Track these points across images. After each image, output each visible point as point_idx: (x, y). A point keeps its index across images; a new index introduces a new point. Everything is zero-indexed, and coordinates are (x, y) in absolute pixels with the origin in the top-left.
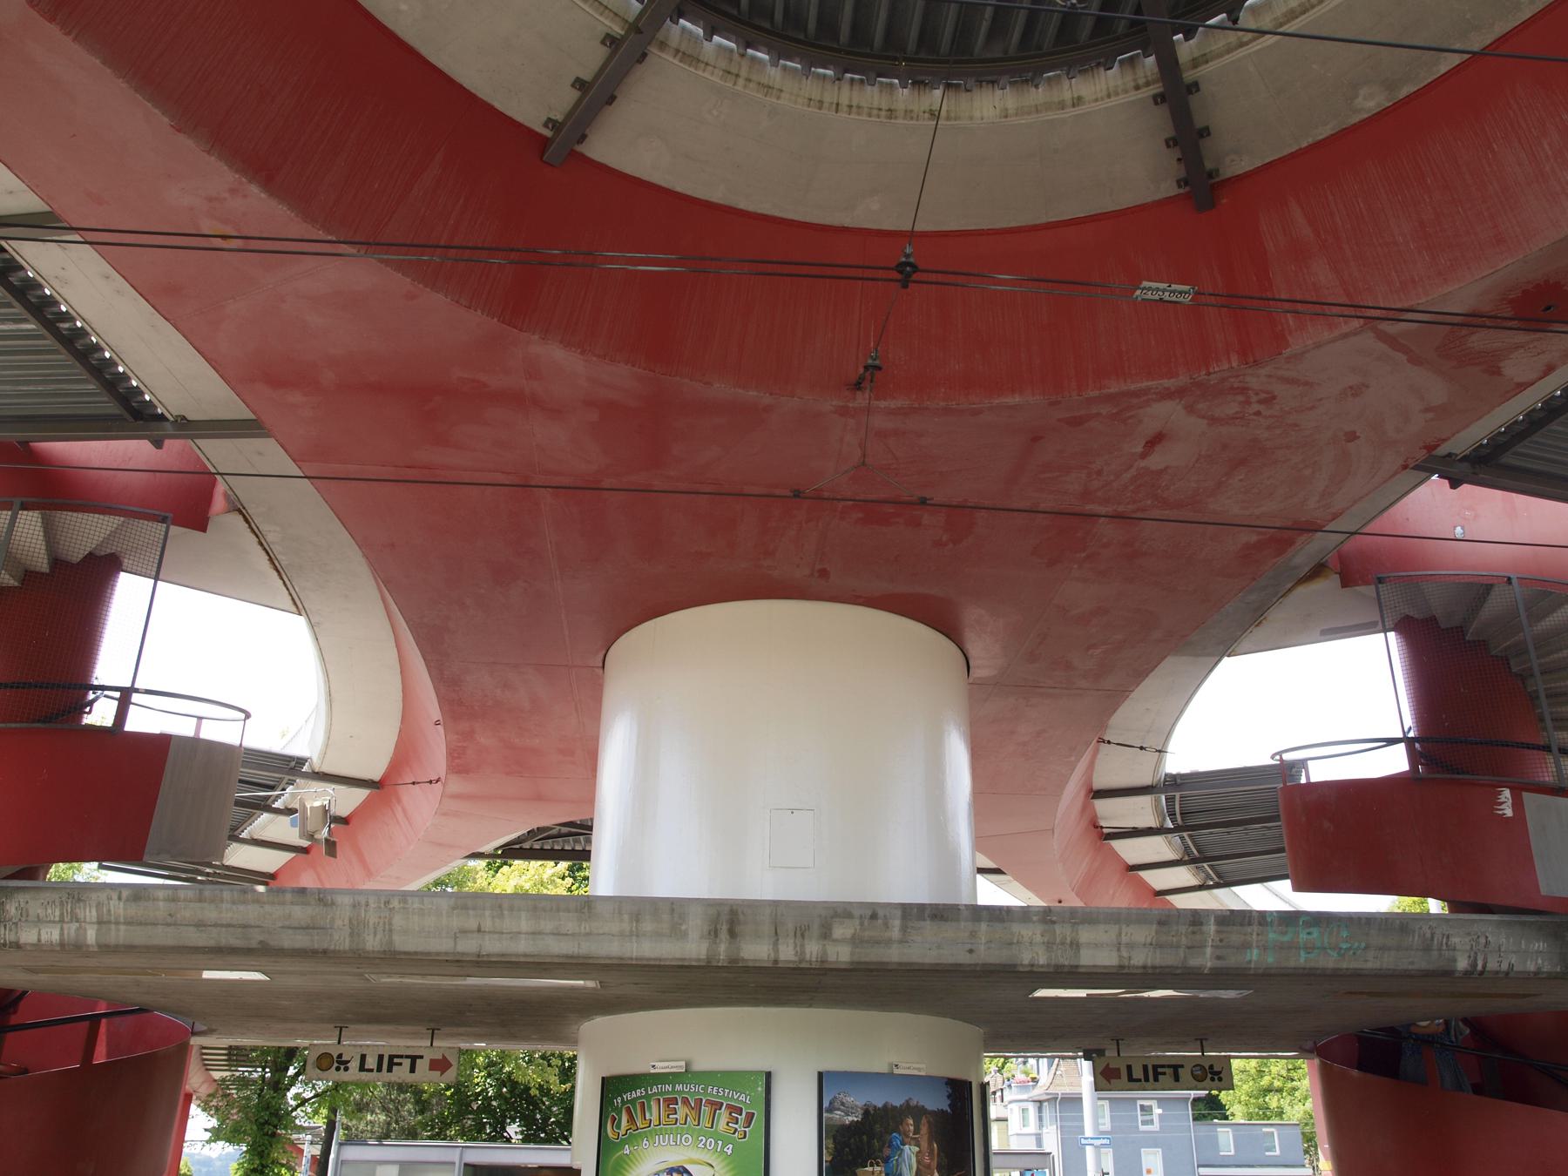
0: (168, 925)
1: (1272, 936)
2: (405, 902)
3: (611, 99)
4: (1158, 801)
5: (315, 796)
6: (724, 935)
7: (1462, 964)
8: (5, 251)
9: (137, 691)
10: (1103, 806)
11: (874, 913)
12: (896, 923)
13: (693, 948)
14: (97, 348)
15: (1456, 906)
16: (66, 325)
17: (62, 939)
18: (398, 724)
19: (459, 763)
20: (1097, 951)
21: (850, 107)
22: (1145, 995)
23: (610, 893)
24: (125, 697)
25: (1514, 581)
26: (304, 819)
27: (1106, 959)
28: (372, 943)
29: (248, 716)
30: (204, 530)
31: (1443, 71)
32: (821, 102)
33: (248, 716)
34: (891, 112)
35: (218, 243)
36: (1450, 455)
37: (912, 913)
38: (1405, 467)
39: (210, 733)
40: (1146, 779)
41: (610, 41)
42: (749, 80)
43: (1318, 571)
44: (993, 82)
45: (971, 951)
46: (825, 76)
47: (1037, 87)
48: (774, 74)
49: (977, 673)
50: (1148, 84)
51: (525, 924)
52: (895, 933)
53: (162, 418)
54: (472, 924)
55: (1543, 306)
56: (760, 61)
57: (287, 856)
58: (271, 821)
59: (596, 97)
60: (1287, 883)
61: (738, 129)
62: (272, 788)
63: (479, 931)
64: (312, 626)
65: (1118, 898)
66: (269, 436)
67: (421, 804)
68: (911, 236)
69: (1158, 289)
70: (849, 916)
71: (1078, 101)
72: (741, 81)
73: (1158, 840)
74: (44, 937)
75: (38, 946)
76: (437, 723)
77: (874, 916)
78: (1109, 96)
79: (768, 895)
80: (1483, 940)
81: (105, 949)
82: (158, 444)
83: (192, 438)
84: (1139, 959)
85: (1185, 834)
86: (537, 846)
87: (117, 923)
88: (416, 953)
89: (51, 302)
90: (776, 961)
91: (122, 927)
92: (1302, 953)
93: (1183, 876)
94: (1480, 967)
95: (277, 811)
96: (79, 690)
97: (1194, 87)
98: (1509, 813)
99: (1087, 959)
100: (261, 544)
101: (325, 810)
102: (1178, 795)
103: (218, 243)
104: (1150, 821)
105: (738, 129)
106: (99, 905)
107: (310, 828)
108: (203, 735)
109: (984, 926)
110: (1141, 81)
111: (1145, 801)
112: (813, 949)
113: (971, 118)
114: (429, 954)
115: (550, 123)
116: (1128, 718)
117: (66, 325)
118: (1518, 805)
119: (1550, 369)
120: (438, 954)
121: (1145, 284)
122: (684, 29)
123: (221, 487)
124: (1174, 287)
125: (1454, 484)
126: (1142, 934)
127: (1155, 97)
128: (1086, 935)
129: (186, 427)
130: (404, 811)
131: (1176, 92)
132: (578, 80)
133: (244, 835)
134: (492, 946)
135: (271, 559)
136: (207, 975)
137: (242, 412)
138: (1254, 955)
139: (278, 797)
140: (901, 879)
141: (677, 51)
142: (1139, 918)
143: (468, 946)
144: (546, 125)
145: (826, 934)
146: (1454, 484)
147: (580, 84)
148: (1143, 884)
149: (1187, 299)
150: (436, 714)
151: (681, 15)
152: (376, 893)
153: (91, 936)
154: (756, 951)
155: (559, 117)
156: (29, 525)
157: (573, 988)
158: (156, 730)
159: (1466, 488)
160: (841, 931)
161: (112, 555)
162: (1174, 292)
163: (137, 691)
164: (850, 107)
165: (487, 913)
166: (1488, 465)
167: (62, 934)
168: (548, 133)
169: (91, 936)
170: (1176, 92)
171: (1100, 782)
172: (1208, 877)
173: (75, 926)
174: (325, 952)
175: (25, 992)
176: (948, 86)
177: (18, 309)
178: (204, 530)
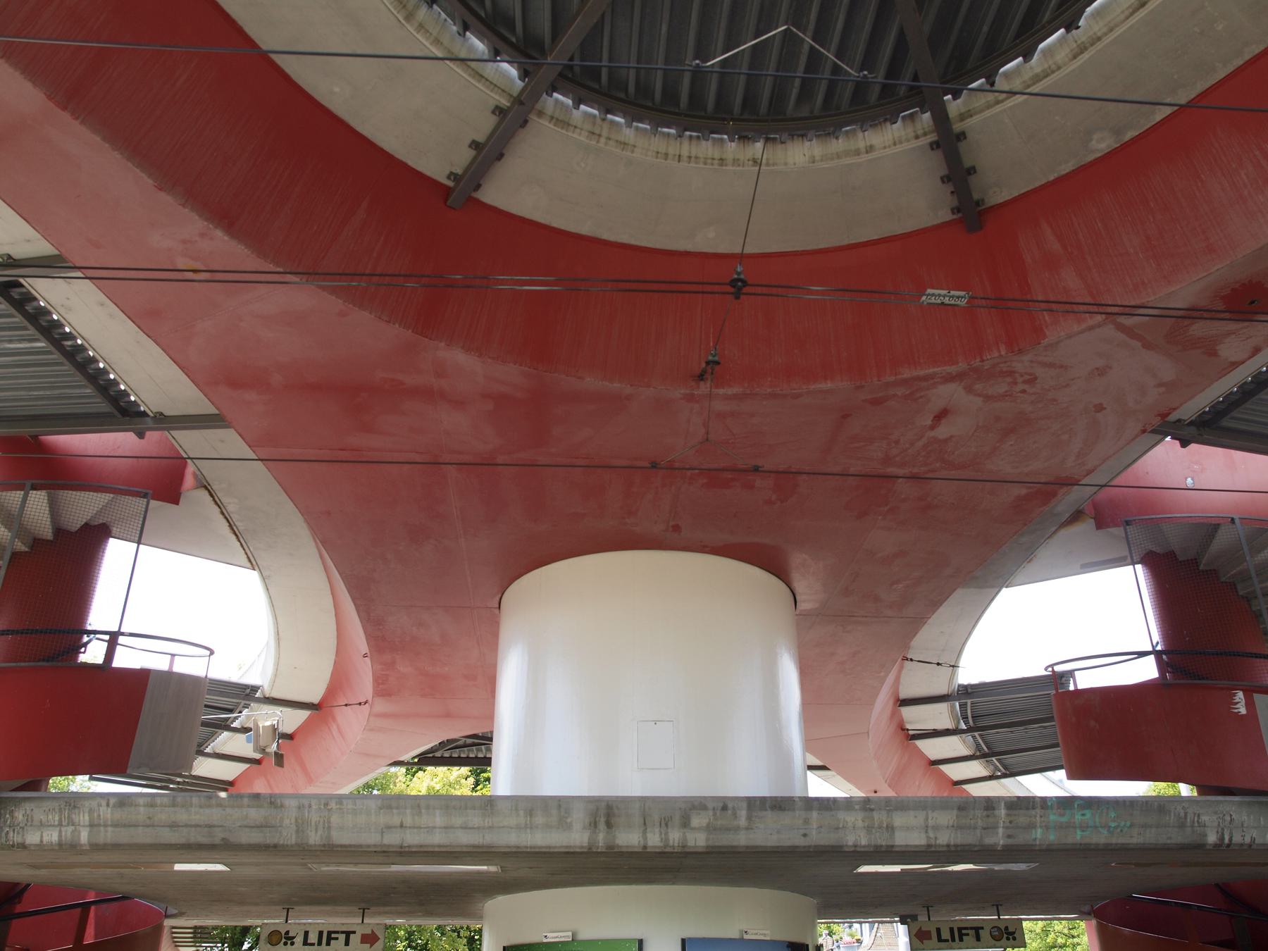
0: (148, 826)
1: (1052, 817)
2: (341, 803)
3: (500, 156)
4: (953, 707)
5: (266, 717)
6: (602, 826)
7: (1212, 838)
8: (22, 286)
9: (123, 634)
10: (907, 712)
11: (724, 805)
12: (743, 813)
13: (577, 837)
14: (94, 360)
15: (1204, 789)
19: (383, 688)
20: (909, 833)
21: (690, 157)
22: (949, 869)
24: (113, 639)
25: (1237, 521)
26: (257, 735)
27: (916, 839)
28: (314, 838)
29: (212, 652)
30: (175, 500)
32: (666, 155)
33: (212, 652)
34: (722, 161)
35: (190, 275)
38: (1144, 431)
39: (181, 667)
40: (943, 690)
41: (499, 111)
42: (609, 139)
43: (1076, 516)
44: (802, 136)
45: (805, 835)
46: (669, 134)
47: (837, 138)
48: (628, 134)
49: (803, 606)
50: (925, 134)
51: (439, 820)
52: (743, 822)
53: (144, 414)
54: (396, 820)
55: (1249, 300)
56: (617, 124)
58: (230, 738)
59: (489, 153)
61: (597, 175)
62: (231, 711)
63: (401, 826)
64: (264, 579)
65: (924, 789)
67: (351, 722)
71: (870, 149)
72: (603, 140)
74: (46, 839)
75: (41, 847)
77: (725, 808)
78: (895, 144)
80: (1228, 818)
81: (96, 847)
82: (141, 435)
83: (168, 429)
84: (944, 839)
86: (447, 755)
87: (105, 826)
88: (350, 846)
90: (645, 847)
91: (110, 829)
93: (976, 768)
94: (1227, 841)
95: (235, 730)
97: (962, 136)
98: (1243, 711)
100: (222, 513)
101: (274, 729)
102: (969, 702)
103: (190, 275)
104: (947, 724)
105: (597, 175)
106: (91, 811)
107: (262, 743)
108: (176, 669)
109: (815, 814)
110: (920, 132)
111: (943, 707)
112: (675, 836)
113: (786, 164)
114: (361, 846)
115: (451, 175)
116: (926, 639)
117: (69, 343)
118: (1250, 704)
119: (1256, 351)
120: (369, 846)
121: (929, 291)
122: (557, 100)
123: (191, 468)
124: (953, 293)
125: (1184, 444)
126: (945, 818)
128: (899, 820)
129: (163, 421)
131: (948, 141)
133: (208, 750)
134: (412, 839)
135: (230, 526)
136: (178, 867)
138: (1038, 833)
139: (236, 718)
140: (746, 777)
141: (552, 118)
142: (942, 805)
143: (392, 839)
144: (449, 178)
145: (685, 824)
146: (1184, 444)
147: (475, 145)
149: (963, 303)
151: (554, 89)
153: (84, 836)
154: (629, 839)
155: (459, 171)
156: (37, 507)
159: (1194, 447)
160: (698, 821)
163: (123, 634)
164: (690, 157)
165: (408, 811)
166: (1211, 428)
167: (60, 836)
168: (450, 184)
169: (84, 836)
170: (948, 141)
171: (905, 693)
172: (997, 769)
173: (70, 829)
174: (275, 846)
176: (767, 140)
177: (32, 331)
178: (175, 500)
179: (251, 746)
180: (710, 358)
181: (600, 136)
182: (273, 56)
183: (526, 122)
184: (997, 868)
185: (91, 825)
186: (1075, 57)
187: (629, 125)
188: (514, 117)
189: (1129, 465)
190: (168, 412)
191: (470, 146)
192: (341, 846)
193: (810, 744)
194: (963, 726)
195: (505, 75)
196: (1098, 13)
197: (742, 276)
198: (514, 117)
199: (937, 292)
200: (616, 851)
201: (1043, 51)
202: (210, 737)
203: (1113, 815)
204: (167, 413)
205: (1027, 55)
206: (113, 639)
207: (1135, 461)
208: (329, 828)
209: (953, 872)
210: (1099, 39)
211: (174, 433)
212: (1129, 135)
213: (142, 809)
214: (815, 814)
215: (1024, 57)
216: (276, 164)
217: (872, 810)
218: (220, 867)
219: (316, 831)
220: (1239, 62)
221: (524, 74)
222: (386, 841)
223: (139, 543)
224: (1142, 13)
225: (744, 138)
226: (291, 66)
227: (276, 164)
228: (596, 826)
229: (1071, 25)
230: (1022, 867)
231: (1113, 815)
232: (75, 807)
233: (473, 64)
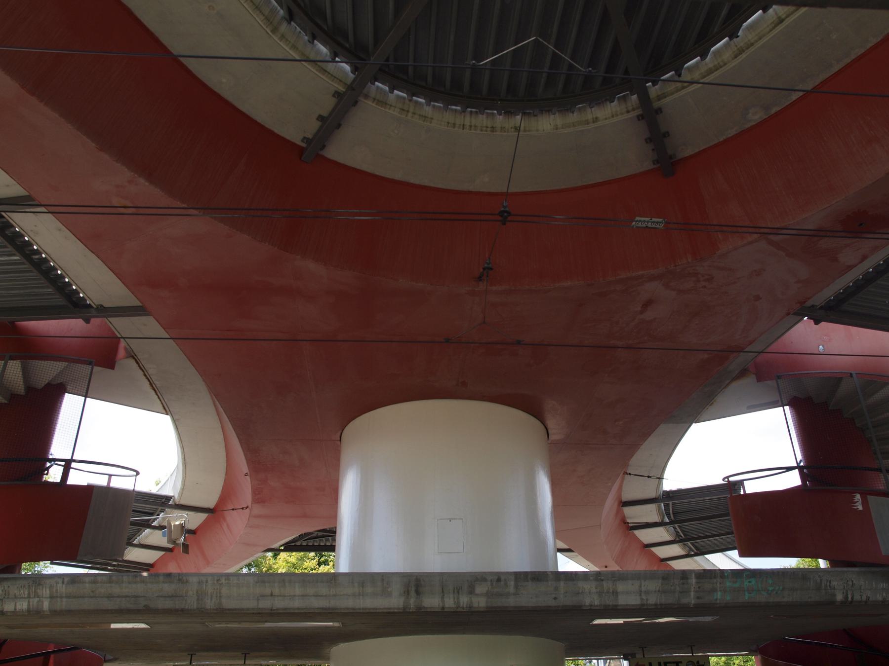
0: (91, 597)
1: (728, 584)
2: (229, 580)
3: (339, 126)
4: (659, 507)
5: (178, 519)
6: (413, 593)
7: (839, 597)
9: (75, 461)
10: (628, 511)
11: (499, 578)
13: (395, 602)
16: (37, 257)
17: (29, 608)
19: (259, 498)
20: (628, 597)
24: (68, 465)
25: (854, 375)
26: (170, 531)
27: (633, 600)
28: (210, 604)
29: (138, 473)
32: (454, 124)
33: (138, 473)
34: (493, 129)
37: (521, 577)
38: (788, 314)
39: (116, 483)
40: (652, 495)
42: (414, 113)
43: (743, 373)
44: (549, 111)
45: (555, 598)
46: (456, 110)
47: (573, 112)
48: (428, 110)
49: (553, 437)
50: (634, 110)
51: (298, 591)
52: (512, 589)
53: (90, 306)
54: (268, 591)
55: (859, 223)
56: (420, 103)
59: (331, 124)
61: (403, 139)
62: (152, 514)
63: (272, 595)
64: (174, 421)
65: (639, 565)
67: (237, 522)
68: (506, 195)
71: (596, 120)
72: (410, 114)
74: (18, 607)
75: (15, 613)
77: (499, 580)
78: (613, 116)
79: (438, 569)
80: (850, 583)
81: (54, 613)
82: (87, 321)
83: (107, 317)
84: (652, 600)
86: (304, 544)
89: (29, 244)
90: (443, 608)
91: (64, 600)
92: (747, 595)
93: (676, 550)
94: (850, 599)
95: (155, 528)
97: (659, 111)
98: (860, 508)
100: (145, 375)
101: (182, 526)
102: (671, 503)
104: (656, 518)
105: (403, 139)
106: (51, 587)
107: (173, 537)
108: (113, 485)
109: (562, 584)
110: (630, 108)
111: (652, 507)
112: (464, 600)
113: (537, 130)
114: (243, 609)
115: (305, 139)
116: (640, 459)
117: (37, 257)
118: (865, 503)
120: (248, 609)
121: (638, 218)
122: (378, 87)
123: (123, 343)
124: (654, 219)
126: (653, 585)
127: (638, 116)
128: (621, 587)
129: (104, 311)
131: (650, 114)
133: (135, 542)
134: (279, 604)
135: (151, 384)
136: (113, 626)
138: (719, 595)
139: (155, 519)
140: (515, 559)
141: (374, 99)
143: (265, 604)
144: (303, 141)
145: (471, 592)
147: (321, 118)
148: (654, 555)
149: (661, 226)
150: (245, 469)
151: (376, 80)
153: (46, 605)
154: (432, 602)
155: (310, 136)
156: (14, 370)
157: (306, 628)
158: (84, 483)
159: (823, 324)
160: (480, 589)
162: (654, 222)
163: (75, 461)
167: (29, 605)
168: (304, 145)
169: (46, 605)
170: (650, 114)
171: (626, 497)
172: (691, 550)
173: (36, 600)
174: (182, 610)
175: (5, 641)
177: (10, 249)
183: (356, 103)
185: (51, 597)
186: (736, 57)
187: (428, 104)
188: (348, 99)
192: (229, 610)
194: (668, 521)
198: (348, 99)
199: (643, 219)
200: (418, 608)
201: (713, 52)
202: (138, 532)
204: (106, 305)
205: (703, 56)
208: (220, 597)
209: (659, 623)
210: (752, 44)
211: (112, 319)
214: (562, 584)
216: (171, 126)
218: (143, 626)
220: (848, 61)
221: (355, 69)
223: (86, 397)
225: (509, 113)
227: (171, 126)
228: (408, 594)
229: (733, 35)
232: (40, 584)
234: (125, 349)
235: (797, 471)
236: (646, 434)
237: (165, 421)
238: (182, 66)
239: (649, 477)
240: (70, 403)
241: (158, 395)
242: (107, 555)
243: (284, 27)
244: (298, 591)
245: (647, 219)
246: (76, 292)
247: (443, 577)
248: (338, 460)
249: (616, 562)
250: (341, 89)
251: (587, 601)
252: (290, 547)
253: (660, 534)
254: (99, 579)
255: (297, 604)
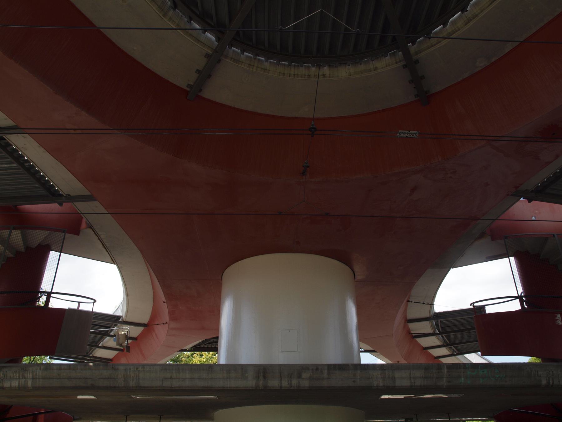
0: (58, 379)
1: (469, 373)
2: (144, 368)
3: (209, 76)
4: (432, 323)
5: (123, 330)
6: (261, 378)
7: (544, 382)
8: (5, 139)
9: (54, 293)
10: (412, 326)
11: (317, 368)
12: (326, 372)
13: (250, 383)
14: (39, 172)
15: (544, 360)
17: (19, 385)
18: (152, 303)
19: (173, 317)
20: (402, 380)
21: (294, 75)
22: (423, 397)
23: (224, 363)
24: (49, 295)
25: (556, 236)
26: (118, 338)
27: (406, 383)
28: (132, 384)
29: (95, 301)
30: (79, 235)
31: (507, 51)
32: (284, 73)
33: (95, 301)
34: (309, 76)
35: (72, 131)
36: (526, 190)
37: (332, 368)
38: (508, 195)
39: (83, 307)
40: (427, 315)
41: (208, 56)
42: (258, 67)
43: (482, 235)
44: (345, 64)
45: (354, 381)
46: (285, 64)
47: (361, 64)
48: (267, 65)
49: (359, 277)
50: (400, 61)
51: (188, 375)
52: (325, 375)
53: (62, 195)
54: (168, 375)
55: (552, 133)
56: (262, 60)
57: (116, 352)
58: (110, 340)
59: (205, 75)
60: (480, 353)
61: (251, 84)
62: (109, 327)
63: (171, 378)
64: (119, 268)
65: (422, 360)
66: (96, 200)
67: (161, 332)
68: (313, 119)
69: (405, 133)
70: (308, 369)
71: (376, 69)
72: (255, 68)
73: (433, 338)
74: (13, 385)
75: (11, 388)
76: (164, 302)
77: (317, 369)
78: (387, 66)
80: (551, 373)
81: (35, 388)
82: (61, 204)
83: (73, 202)
84: (418, 383)
85: (443, 335)
86: (206, 347)
87: (39, 379)
88: (148, 387)
89: (22, 156)
90: (281, 387)
91: (41, 380)
92: (481, 379)
93: (444, 351)
94: (551, 383)
95: (112, 336)
96: (36, 291)
97: (417, 62)
99: (398, 383)
100: (99, 239)
101: (125, 335)
102: (439, 320)
103: (72, 131)
105: (251, 84)
106: (33, 372)
107: (120, 341)
108: (81, 308)
109: (358, 372)
110: (398, 61)
111: (427, 323)
112: (295, 382)
113: (338, 77)
114: (153, 387)
115: (189, 86)
116: (417, 291)
119: (557, 157)
120: (156, 387)
121: (400, 131)
122: (234, 50)
125: (530, 201)
126: (418, 373)
127: (403, 66)
128: (397, 374)
129: (70, 198)
130: (156, 335)
131: (410, 64)
132: (197, 70)
133: (100, 345)
134: (176, 384)
135: (103, 245)
136: (79, 397)
137: (86, 192)
138: (462, 380)
140: (332, 355)
141: (232, 58)
142: (427, 368)
143: (167, 384)
144: (187, 87)
145: (299, 376)
146: (530, 201)
147: (198, 71)
148: (430, 355)
149: (417, 136)
150: (164, 299)
151: (232, 46)
152: (133, 365)
153: (30, 383)
154: (274, 383)
155: (192, 84)
156: (16, 236)
157: (208, 399)
160: (305, 375)
161: (48, 244)
162: (411, 134)
163: (54, 293)
164: (294, 75)
165: (174, 371)
166: (540, 193)
167: (19, 383)
168: (188, 89)
169: (30, 383)
170: (410, 64)
171: (410, 316)
172: (454, 351)
173: (24, 380)
174: (115, 387)
175: (11, 407)
176: (329, 66)
177: (10, 159)
179: (115, 343)
180: (305, 164)
181: (254, 66)
182: (101, 30)
183: (219, 61)
184: (432, 396)
185: (33, 378)
186: (466, 24)
187: (267, 61)
188: (215, 59)
189: (505, 211)
190: (72, 194)
191: (196, 72)
192: (144, 387)
193: (361, 339)
194: (438, 332)
195: (210, 39)
196: (475, 4)
197: (314, 126)
198: (215, 59)
199: (404, 131)
200: (264, 386)
201: (451, 22)
202: (101, 339)
203: (497, 371)
204: (72, 194)
205: (445, 24)
206: (49, 295)
207: (507, 209)
208: (139, 379)
210: (477, 16)
211: (76, 204)
212: (494, 59)
213: (55, 371)
214: (358, 372)
215: (443, 25)
216: (105, 79)
217: (385, 370)
218: (92, 397)
219: (133, 380)
220: (542, 24)
221: (218, 39)
222: (164, 385)
223: (61, 253)
224: (495, 4)
225: (319, 66)
226: (110, 34)
227: (105, 79)
228: (259, 378)
230: (456, 396)
231: (497, 371)
232: (26, 370)
233: (190, 31)
234: (86, 223)
235: (518, 300)
236: (418, 275)
237: (113, 268)
238: (105, 37)
239: (424, 303)
240: (53, 255)
241: (108, 253)
242: (82, 354)
243: (171, 13)
244: (188, 375)
245: (407, 131)
246: (53, 187)
247: (281, 367)
248: (220, 292)
249: (405, 359)
250: (210, 52)
251: (375, 384)
252: (195, 349)
253: (433, 341)
254: (63, 367)
255: (187, 384)
